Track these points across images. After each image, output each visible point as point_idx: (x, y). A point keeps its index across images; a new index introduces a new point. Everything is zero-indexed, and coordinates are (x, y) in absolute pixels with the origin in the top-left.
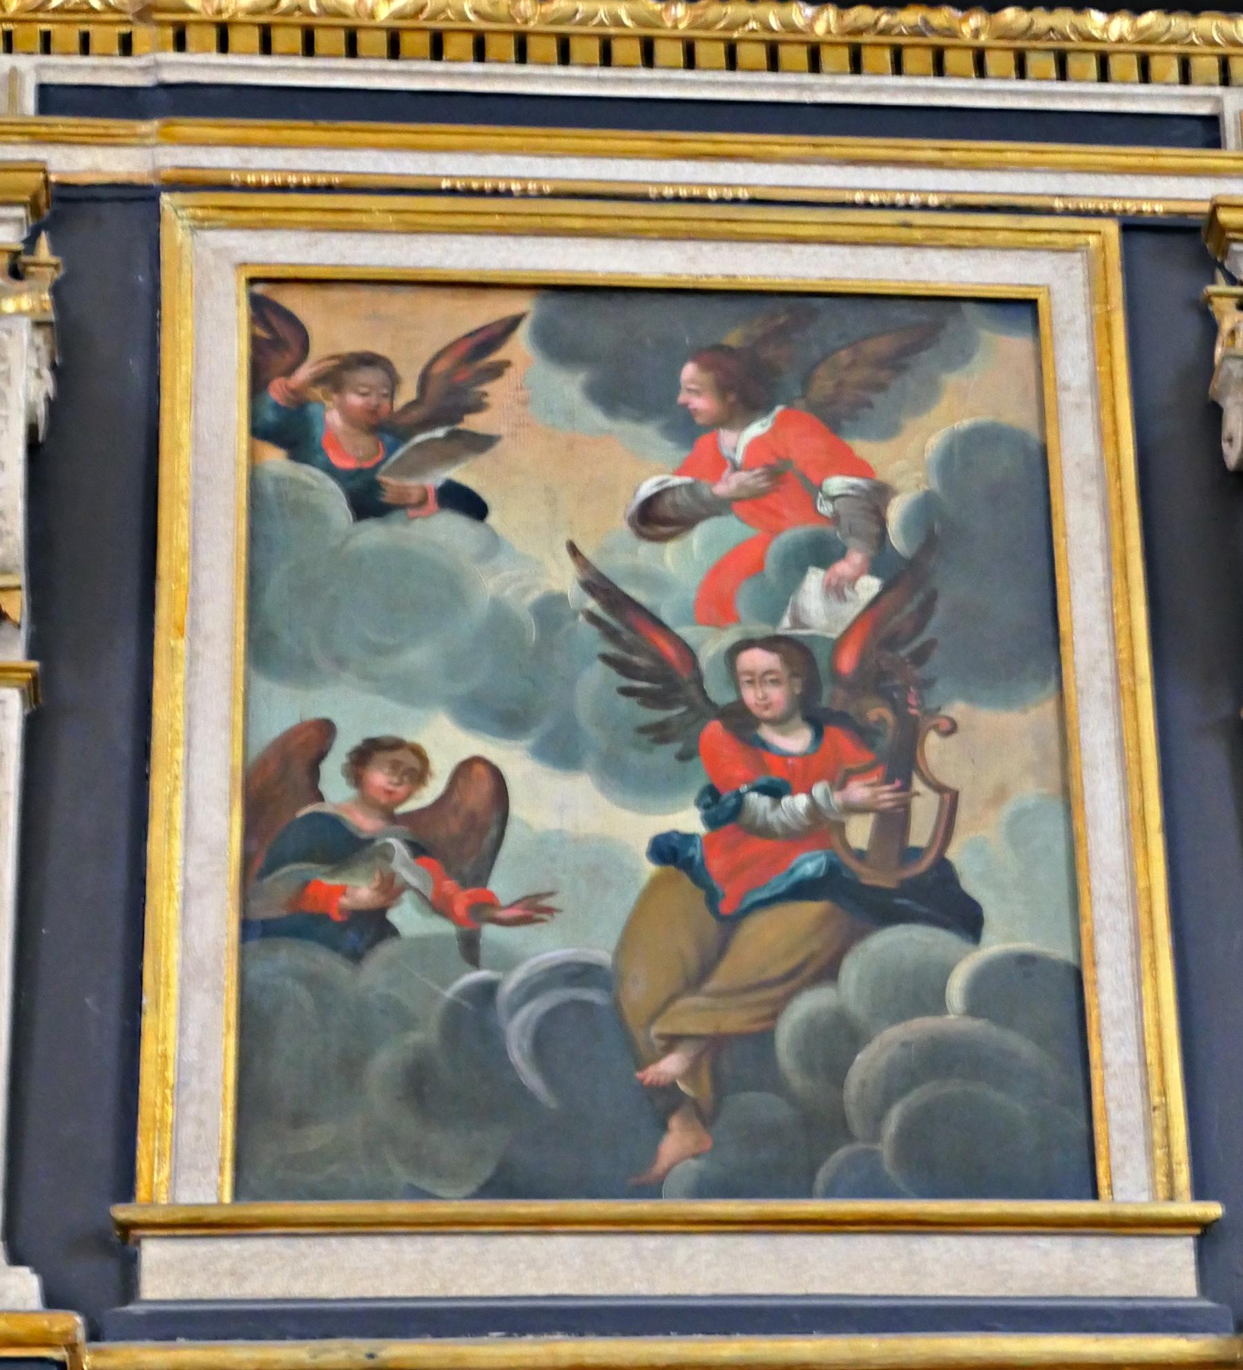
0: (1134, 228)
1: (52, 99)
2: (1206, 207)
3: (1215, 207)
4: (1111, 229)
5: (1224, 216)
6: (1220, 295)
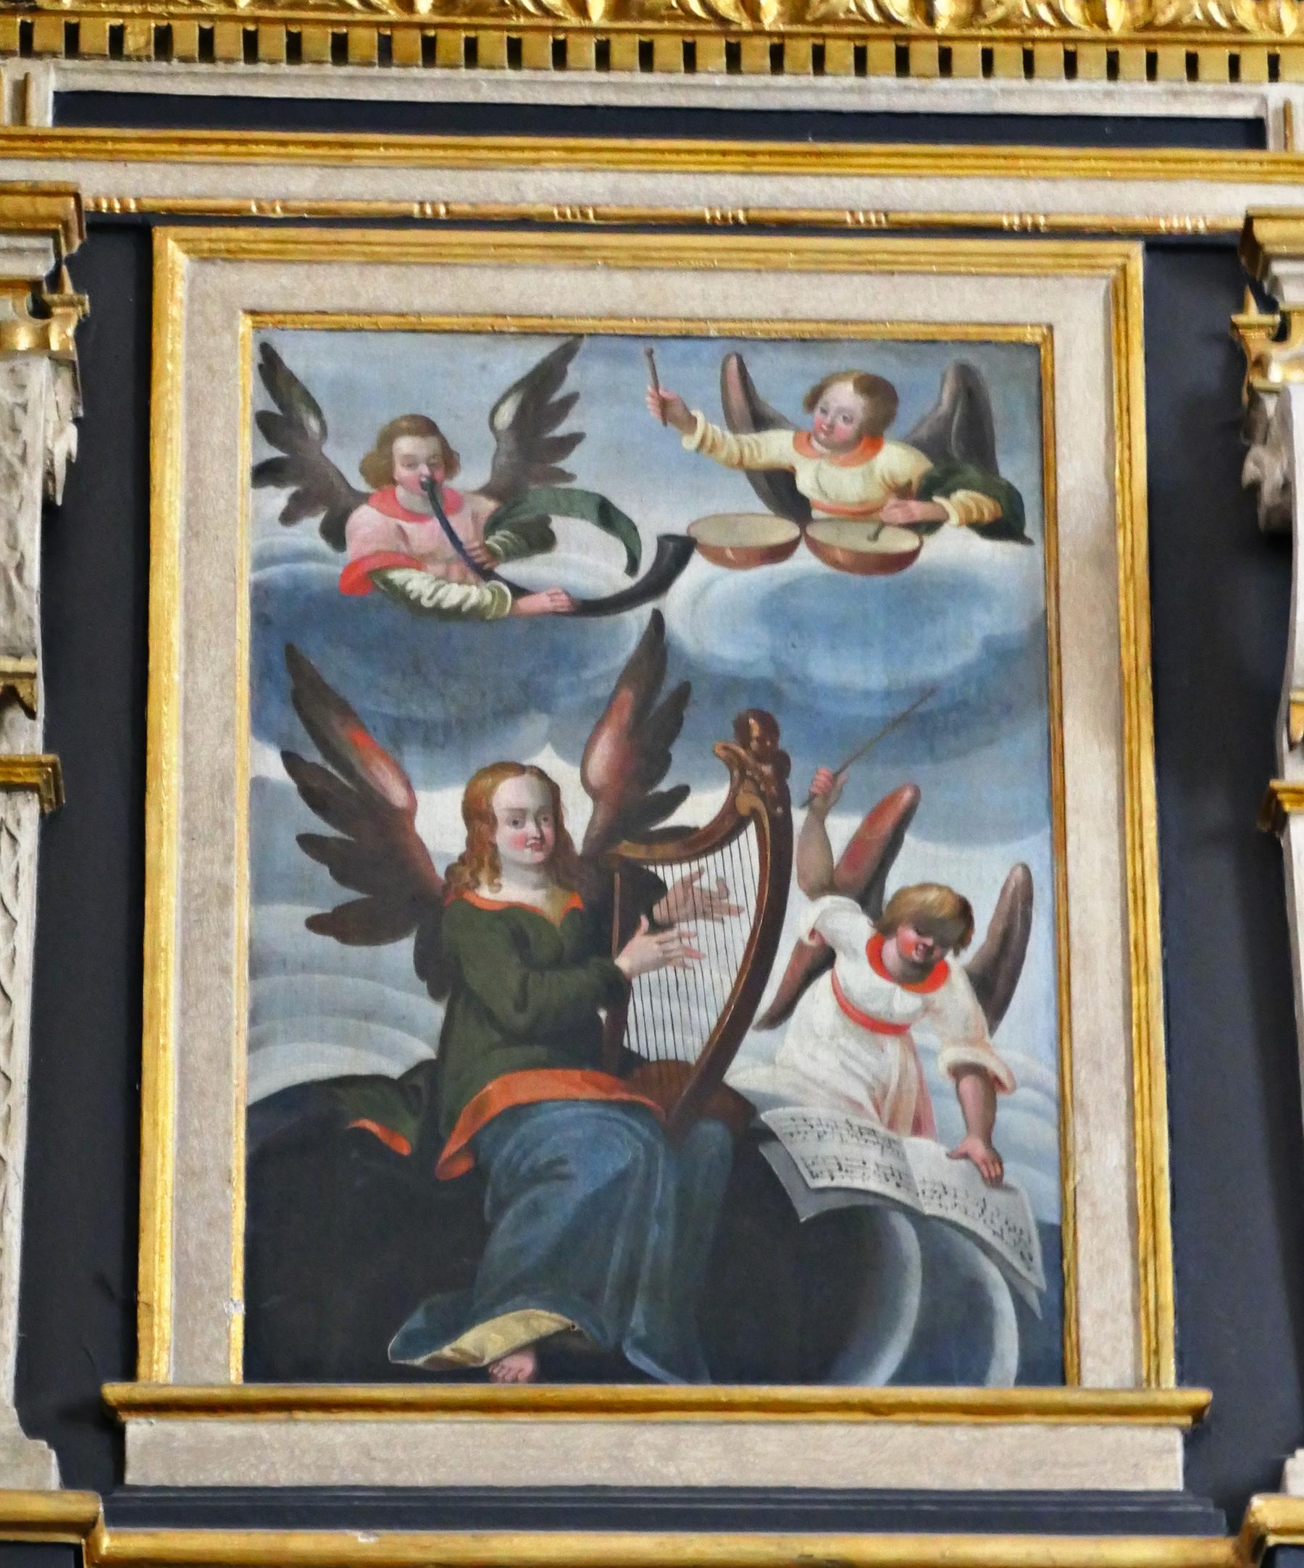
0: (1167, 250)
1: (72, 107)
2: (1238, 223)
3: (1249, 221)
4: (1136, 250)
5: (1263, 231)
6: (1250, 327)
